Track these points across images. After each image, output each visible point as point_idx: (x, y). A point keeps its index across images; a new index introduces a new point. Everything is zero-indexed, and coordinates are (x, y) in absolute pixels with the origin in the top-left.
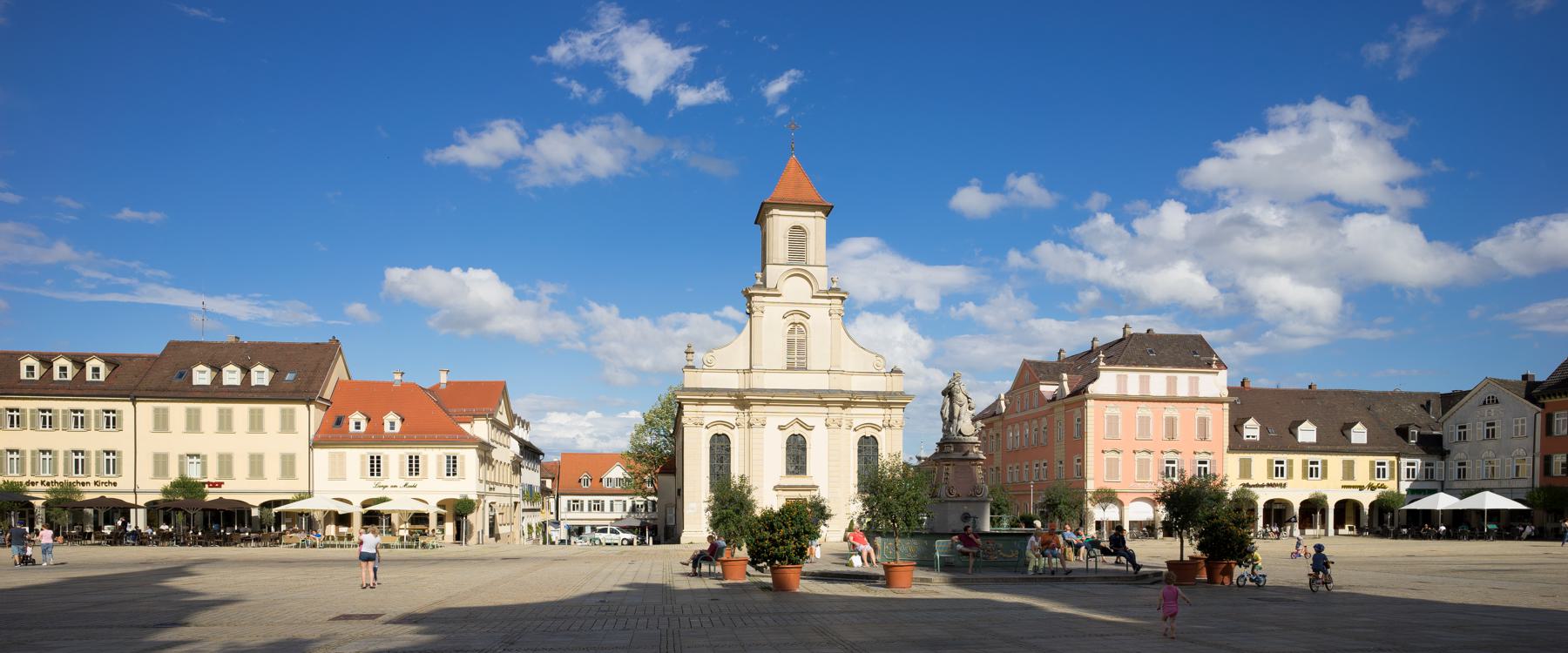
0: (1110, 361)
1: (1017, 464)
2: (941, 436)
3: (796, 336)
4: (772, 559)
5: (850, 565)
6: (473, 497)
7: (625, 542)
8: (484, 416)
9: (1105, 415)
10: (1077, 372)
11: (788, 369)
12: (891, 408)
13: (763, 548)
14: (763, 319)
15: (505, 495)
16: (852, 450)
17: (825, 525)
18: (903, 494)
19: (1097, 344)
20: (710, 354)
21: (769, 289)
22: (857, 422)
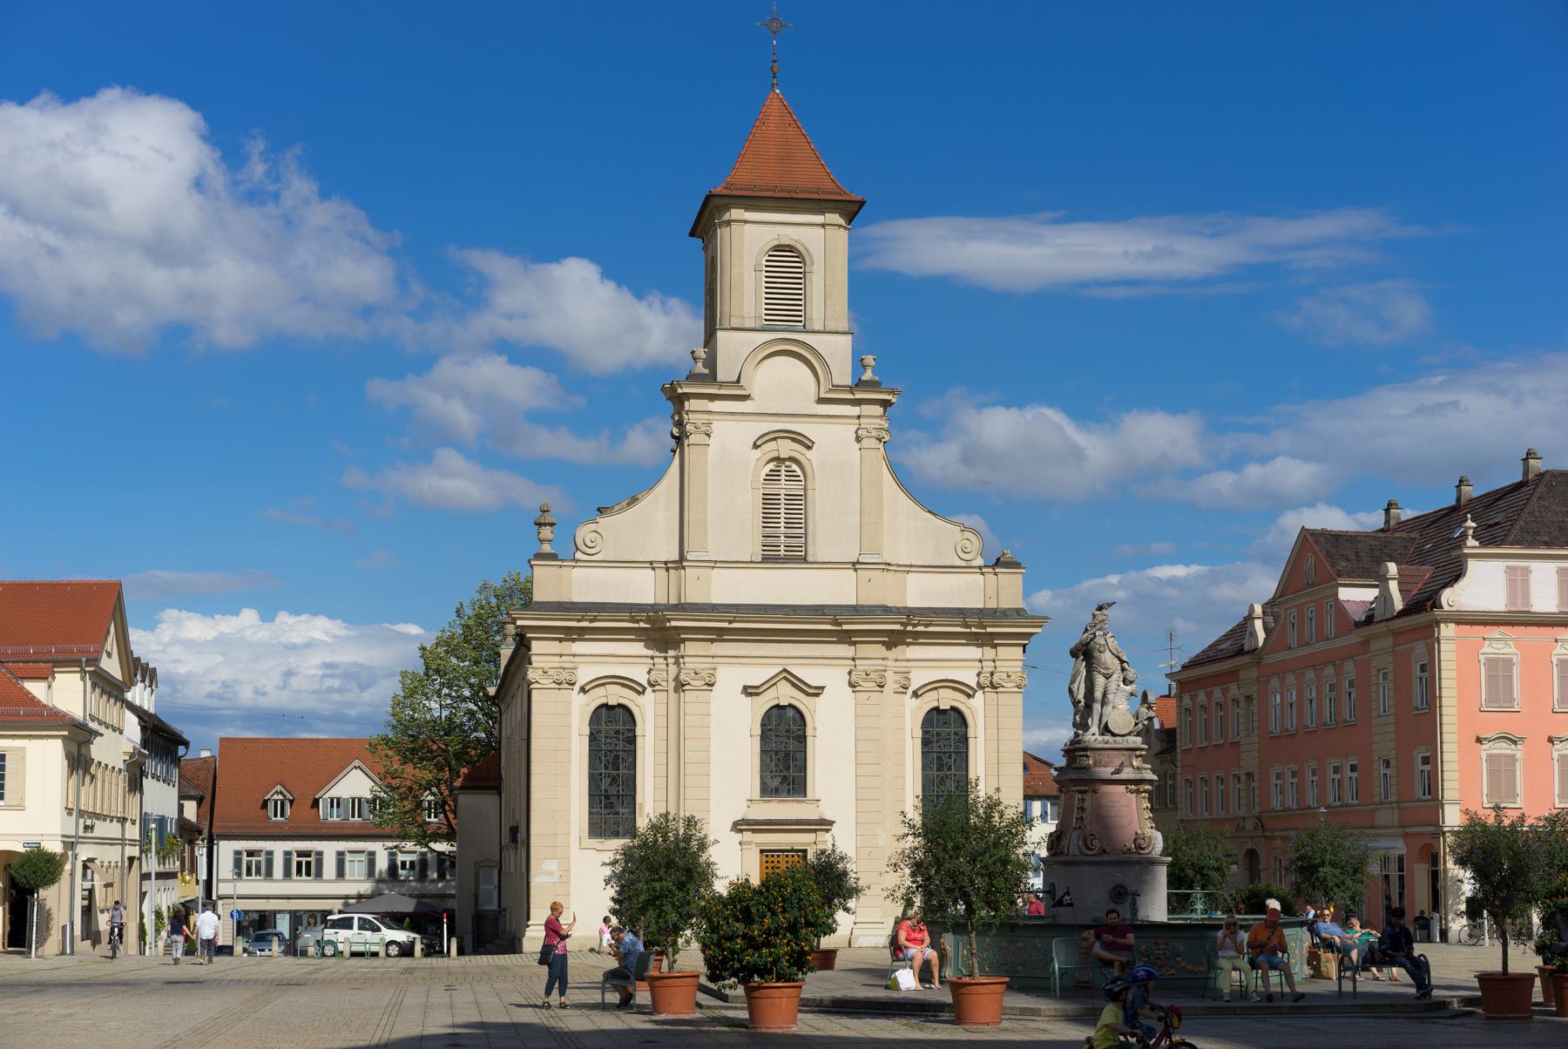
0: (1492, 536)
1: (1295, 767)
2: (1247, 614)
3: (783, 487)
4: (745, 974)
5: (895, 986)
6: (55, 847)
7: (394, 950)
8: (77, 663)
9: (1482, 658)
10: (1420, 558)
11: (765, 559)
12: (995, 646)
13: (733, 952)
14: (710, 448)
15: (110, 841)
16: (909, 741)
17: (847, 910)
18: (982, 854)
19: (1470, 492)
20: (593, 527)
21: (722, 385)
22: (919, 678)
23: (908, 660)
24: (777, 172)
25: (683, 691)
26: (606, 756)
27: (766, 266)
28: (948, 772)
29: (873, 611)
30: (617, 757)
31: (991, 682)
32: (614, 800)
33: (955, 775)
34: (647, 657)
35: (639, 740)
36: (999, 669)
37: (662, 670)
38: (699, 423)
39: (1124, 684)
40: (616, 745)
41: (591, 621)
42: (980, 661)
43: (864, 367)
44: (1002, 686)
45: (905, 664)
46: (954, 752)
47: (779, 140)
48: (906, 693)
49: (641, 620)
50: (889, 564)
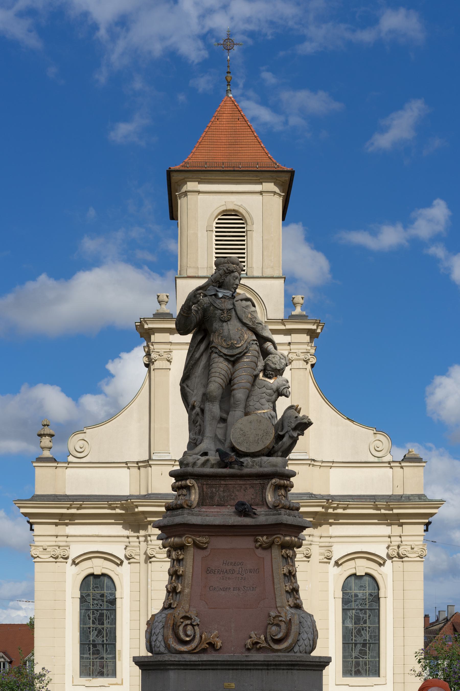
12: (401, 525)
16: (331, 601)
20: (81, 436)
23: (331, 537)
24: (226, 154)
25: (150, 562)
26: (93, 613)
27: (216, 228)
28: (364, 625)
29: (301, 497)
30: (102, 615)
31: (398, 554)
32: (99, 647)
33: (369, 627)
34: (123, 536)
35: (118, 602)
36: (404, 543)
37: (136, 547)
38: (162, 352)
39: (265, 375)
40: (101, 605)
41: (78, 509)
42: (389, 537)
43: (295, 305)
44: (407, 557)
45: (328, 540)
46: (368, 609)
47: (229, 130)
48: (329, 563)
49: (117, 507)
50: (314, 460)
